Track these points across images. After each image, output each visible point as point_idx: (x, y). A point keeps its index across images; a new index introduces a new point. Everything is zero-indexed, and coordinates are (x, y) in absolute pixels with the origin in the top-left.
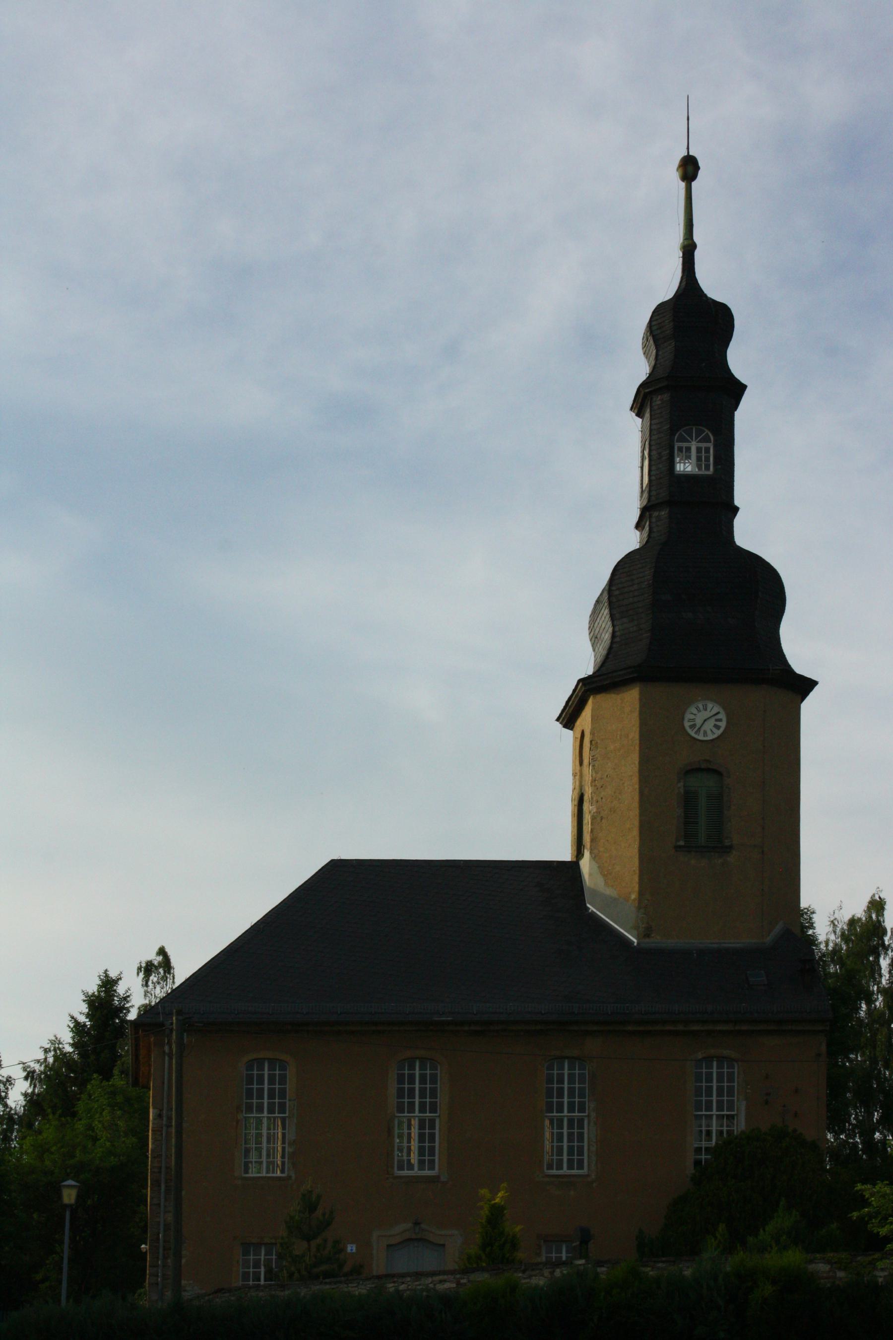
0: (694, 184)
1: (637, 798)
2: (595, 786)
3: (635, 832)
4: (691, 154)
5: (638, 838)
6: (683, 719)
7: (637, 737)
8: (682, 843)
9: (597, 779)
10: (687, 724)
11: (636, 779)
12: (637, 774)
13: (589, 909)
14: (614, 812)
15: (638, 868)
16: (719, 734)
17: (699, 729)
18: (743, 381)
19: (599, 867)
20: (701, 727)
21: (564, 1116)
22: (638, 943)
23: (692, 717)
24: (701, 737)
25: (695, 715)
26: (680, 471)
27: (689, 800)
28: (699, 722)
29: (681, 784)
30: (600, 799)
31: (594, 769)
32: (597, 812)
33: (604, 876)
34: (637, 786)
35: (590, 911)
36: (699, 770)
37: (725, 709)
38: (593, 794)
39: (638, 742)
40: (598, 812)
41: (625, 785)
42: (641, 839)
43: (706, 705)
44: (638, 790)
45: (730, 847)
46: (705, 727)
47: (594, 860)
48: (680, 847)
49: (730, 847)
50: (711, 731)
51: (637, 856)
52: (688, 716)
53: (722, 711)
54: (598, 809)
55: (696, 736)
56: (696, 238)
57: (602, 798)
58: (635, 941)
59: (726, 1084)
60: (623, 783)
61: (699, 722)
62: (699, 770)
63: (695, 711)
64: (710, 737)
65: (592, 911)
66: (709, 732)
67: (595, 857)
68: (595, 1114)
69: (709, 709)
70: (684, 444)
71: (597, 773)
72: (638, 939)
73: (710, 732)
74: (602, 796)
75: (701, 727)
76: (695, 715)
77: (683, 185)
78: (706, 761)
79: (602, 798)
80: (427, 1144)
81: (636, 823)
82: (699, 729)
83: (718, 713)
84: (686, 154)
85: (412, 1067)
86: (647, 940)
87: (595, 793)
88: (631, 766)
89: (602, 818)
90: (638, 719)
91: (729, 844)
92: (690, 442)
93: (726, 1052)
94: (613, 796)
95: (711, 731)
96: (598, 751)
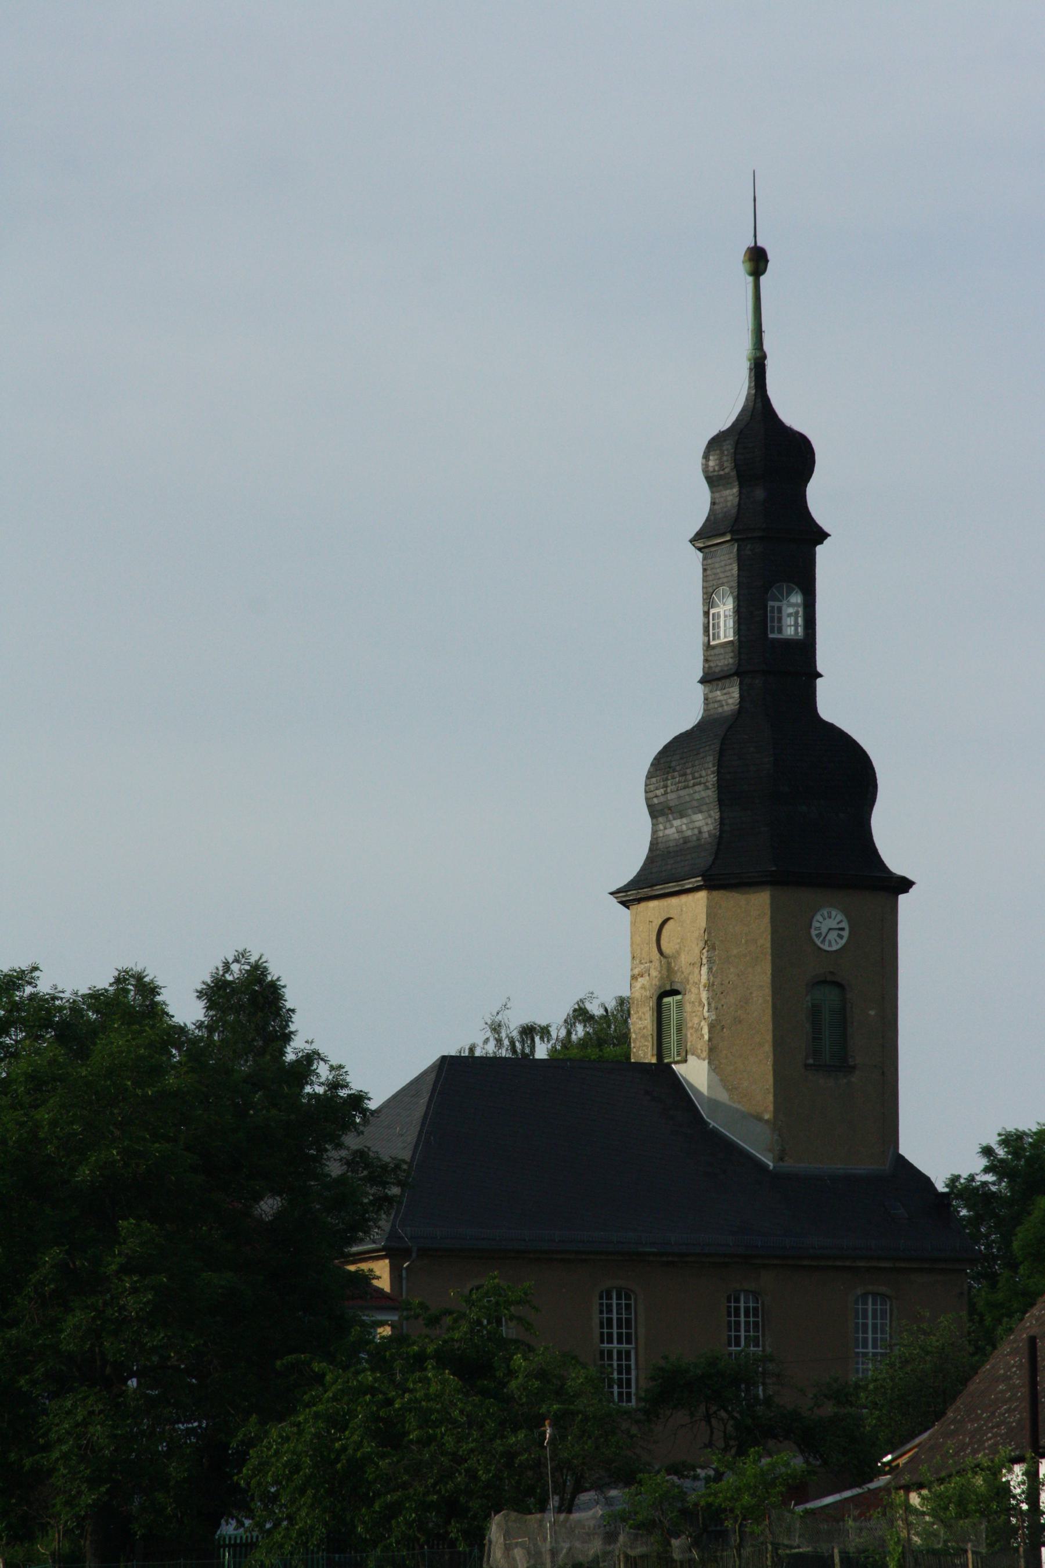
0: (762, 278)
1: (769, 1011)
2: (713, 990)
3: (768, 1048)
4: (759, 244)
5: (771, 1055)
6: (810, 927)
7: (769, 945)
8: (811, 1061)
9: (716, 983)
10: (814, 933)
11: (768, 991)
12: (769, 986)
13: (710, 1124)
14: (740, 1022)
15: (772, 1087)
16: (843, 944)
17: (825, 938)
18: (826, 528)
19: (721, 1080)
20: (826, 935)
21: (615, 1348)
22: (774, 1167)
23: (818, 925)
24: (826, 947)
25: (821, 922)
26: (791, 635)
27: (815, 1012)
28: (824, 931)
29: (808, 998)
30: (720, 1006)
31: (712, 972)
32: (716, 1020)
33: (728, 1090)
34: (769, 999)
35: (711, 1126)
36: (825, 982)
37: (847, 916)
38: (711, 1000)
39: (769, 951)
40: (718, 1020)
41: (754, 995)
42: (775, 1055)
43: (830, 912)
44: (770, 1002)
45: (854, 1068)
46: (830, 937)
47: (715, 1072)
48: (811, 1065)
49: (854, 1068)
50: (836, 941)
51: (772, 1073)
52: (815, 924)
53: (845, 920)
54: (717, 1016)
55: (822, 946)
56: (766, 347)
57: (723, 1006)
58: (771, 1164)
59: (879, 1321)
60: (751, 993)
61: (824, 931)
62: (825, 982)
63: (821, 919)
64: (835, 948)
65: (713, 1126)
66: (833, 942)
67: (716, 1068)
68: (390, 1333)
69: (833, 917)
70: (776, 603)
71: (715, 977)
72: (773, 1162)
73: (834, 943)
74: (722, 1003)
75: (826, 935)
76: (821, 922)
77: (750, 279)
78: (831, 973)
79: (723, 1006)
80: (624, 1376)
81: (769, 1037)
82: (825, 938)
83: (841, 921)
84: (753, 245)
85: (865, 1303)
86: (781, 1164)
87: (713, 999)
88: (762, 975)
89: (723, 1028)
90: (769, 925)
91: (853, 1063)
92: (781, 601)
93: (883, 1289)
94: (737, 1005)
95: (836, 941)
96: (716, 953)
